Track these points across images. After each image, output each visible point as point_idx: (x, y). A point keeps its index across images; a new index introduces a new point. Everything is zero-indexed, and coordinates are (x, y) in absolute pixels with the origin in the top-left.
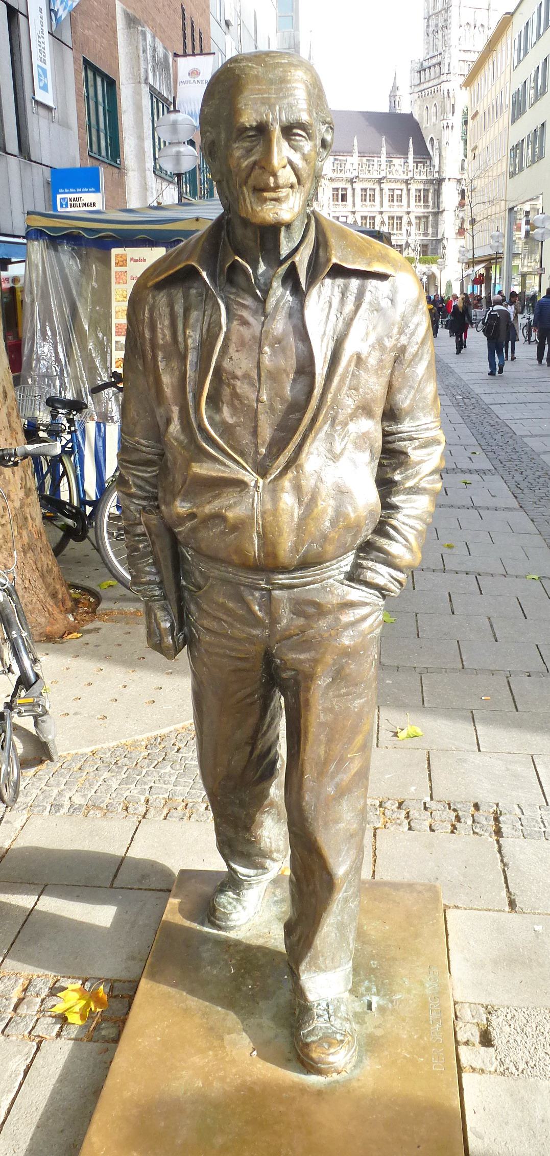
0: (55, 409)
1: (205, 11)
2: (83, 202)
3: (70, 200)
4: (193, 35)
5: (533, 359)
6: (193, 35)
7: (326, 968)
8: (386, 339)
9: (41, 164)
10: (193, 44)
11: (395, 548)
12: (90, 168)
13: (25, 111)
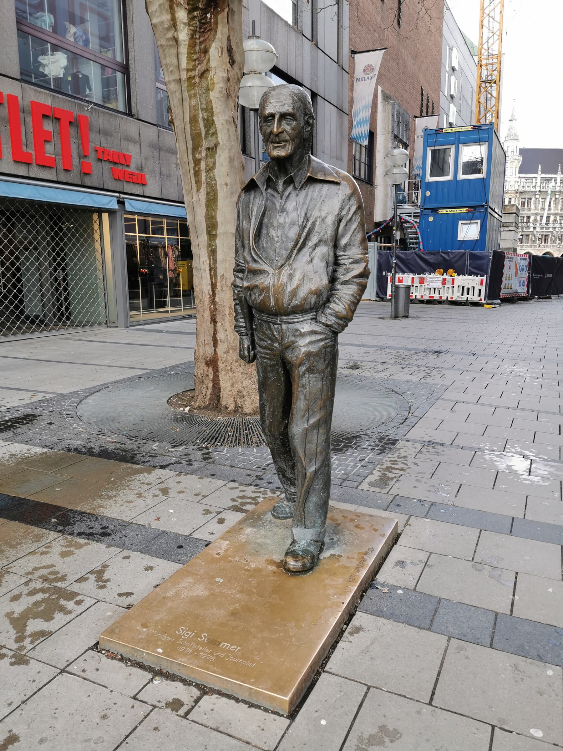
0: (341, 318)
1: (437, 89)
5: (508, 258)
12: (330, 456)
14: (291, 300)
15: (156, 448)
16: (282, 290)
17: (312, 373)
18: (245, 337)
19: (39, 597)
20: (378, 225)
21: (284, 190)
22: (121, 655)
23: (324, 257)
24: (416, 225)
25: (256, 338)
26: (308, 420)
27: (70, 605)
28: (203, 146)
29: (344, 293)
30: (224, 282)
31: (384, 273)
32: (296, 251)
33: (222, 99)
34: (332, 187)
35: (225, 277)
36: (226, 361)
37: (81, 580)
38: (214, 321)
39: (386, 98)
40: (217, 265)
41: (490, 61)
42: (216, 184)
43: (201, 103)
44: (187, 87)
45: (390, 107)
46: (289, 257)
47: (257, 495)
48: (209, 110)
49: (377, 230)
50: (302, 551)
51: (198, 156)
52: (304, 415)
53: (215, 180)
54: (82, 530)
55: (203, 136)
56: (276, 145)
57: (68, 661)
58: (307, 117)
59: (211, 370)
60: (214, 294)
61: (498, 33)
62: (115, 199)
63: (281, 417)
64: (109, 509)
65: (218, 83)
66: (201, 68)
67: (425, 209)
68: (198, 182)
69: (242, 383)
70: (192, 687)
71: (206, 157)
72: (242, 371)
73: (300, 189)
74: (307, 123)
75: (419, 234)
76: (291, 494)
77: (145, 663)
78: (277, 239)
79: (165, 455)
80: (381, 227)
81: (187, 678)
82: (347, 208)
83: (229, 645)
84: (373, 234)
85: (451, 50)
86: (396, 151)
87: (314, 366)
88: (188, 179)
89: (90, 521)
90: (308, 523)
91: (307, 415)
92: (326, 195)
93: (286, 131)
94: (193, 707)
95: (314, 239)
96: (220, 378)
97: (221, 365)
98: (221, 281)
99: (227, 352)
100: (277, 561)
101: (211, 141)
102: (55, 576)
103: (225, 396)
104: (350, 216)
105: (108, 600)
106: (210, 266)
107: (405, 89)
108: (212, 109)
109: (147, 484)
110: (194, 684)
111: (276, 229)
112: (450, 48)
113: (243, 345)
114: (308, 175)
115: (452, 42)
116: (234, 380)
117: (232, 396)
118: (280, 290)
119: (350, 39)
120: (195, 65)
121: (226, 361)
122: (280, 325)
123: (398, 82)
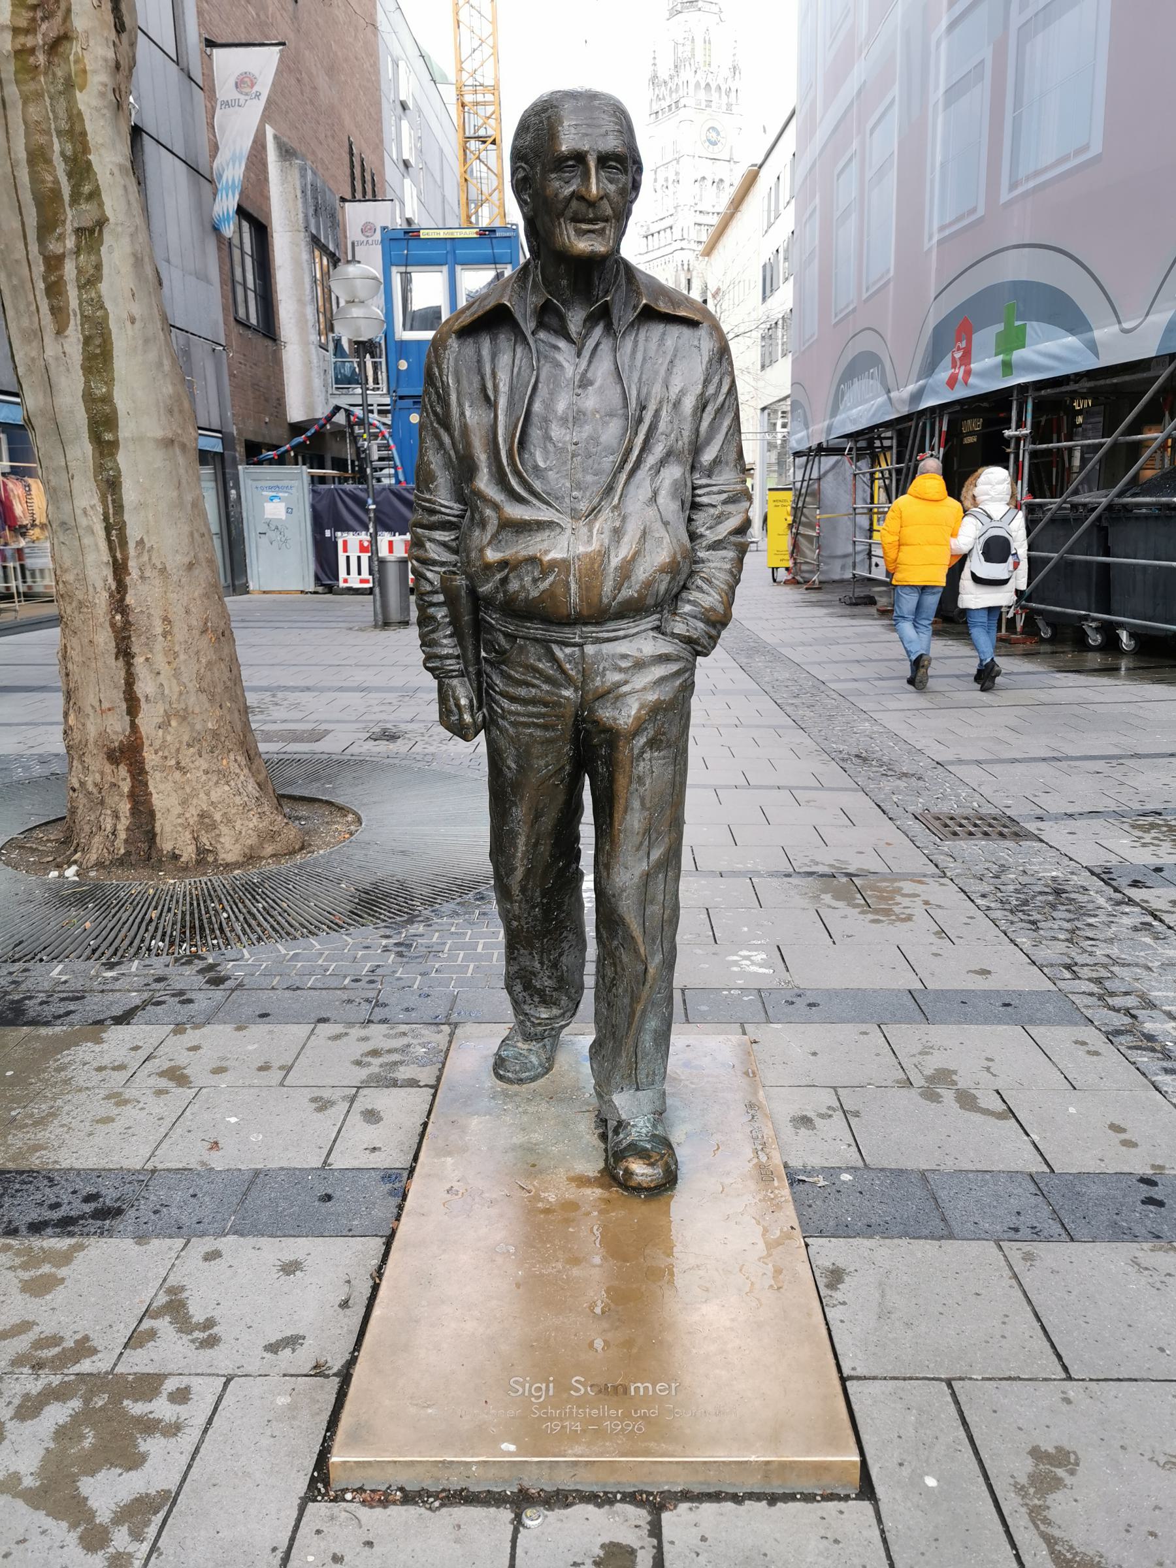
4: (363, 177)
6: (363, 177)
7: (705, 647)
10: (364, 188)
14: (618, 587)
15: (64, 978)
17: (659, 749)
19: (57, 1414)
20: (297, 429)
21: (586, 336)
22: (401, 1489)
23: (676, 486)
24: (386, 432)
26: (649, 854)
27: (161, 1408)
28: (68, 222)
30: (145, 558)
31: (328, 533)
32: (623, 477)
33: (105, 111)
34: (686, 331)
35: (148, 545)
36: (164, 745)
37: (135, 1340)
38: (125, 653)
39: (287, 153)
40: (126, 517)
41: (480, 98)
42: (106, 317)
43: (56, 118)
44: (16, 73)
45: (296, 174)
46: (609, 489)
47: (404, 1041)
48: (76, 134)
49: (301, 438)
50: (649, 1142)
51: (54, 247)
52: (641, 843)
53: (102, 307)
54: (34, 1215)
55: (66, 198)
56: (584, 226)
57: (274, 1549)
59: (123, 771)
60: (122, 587)
61: (490, 41)
63: (551, 856)
64: (64, 1150)
65: (95, 72)
66: (48, 30)
67: (401, 398)
68: (59, 312)
69: (208, 794)
70: (618, 1505)
71: (77, 252)
72: (205, 766)
75: (394, 450)
76: (539, 1024)
77: (475, 1489)
79: (103, 991)
80: (309, 434)
81: (595, 1489)
82: (716, 380)
83: (650, 1386)
84: (293, 448)
85: (396, 64)
87: (664, 734)
88: (29, 304)
89: (38, 1189)
90: (642, 1077)
91: (646, 843)
92: (676, 350)
94: (659, 1548)
95: (658, 450)
96: (151, 789)
97: (150, 757)
98: (139, 556)
99: (164, 725)
100: (591, 1174)
101: (86, 214)
102: (57, 1350)
103: (168, 829)
104: (721, 398)
105: (249, 1369)
106: (106, 518)
108: (84, 134)
109: (114, 1069)
110: (619, 1496)
112: (393, 60)
114: (644, 301)
115: (397, 50)
116: (188, 790)
117: (186, 826)
118: (596, 566)
119: (200, 13)
120: (34, 20)
121: (164, 745)
122: (581, 646)
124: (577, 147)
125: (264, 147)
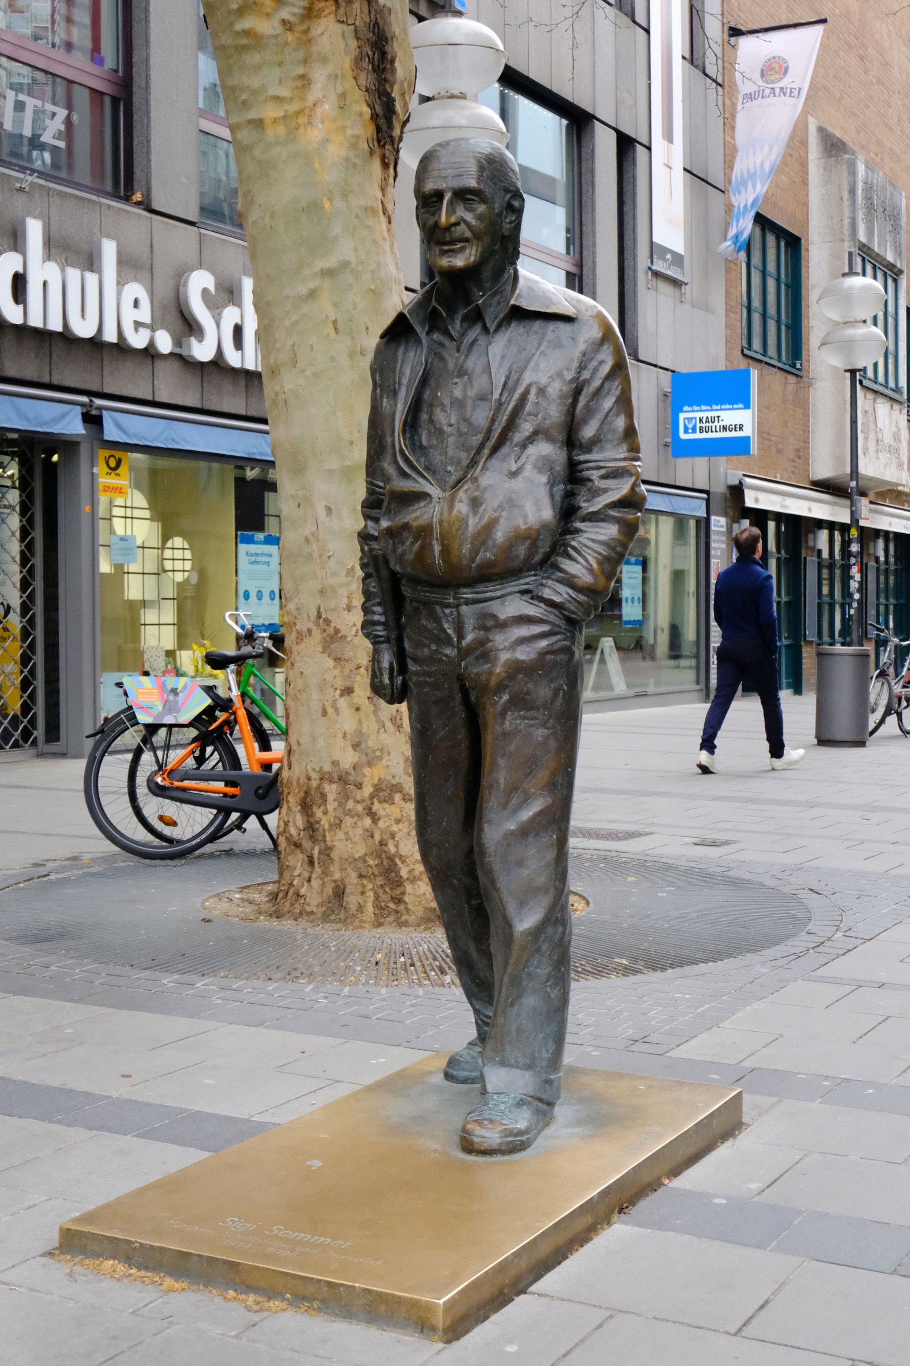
2: (721, 423)
3: (701, 420)
8: (566, 373)
9: (655, 366)
11: (568, 566)
13: (635, 285)
14: (475, 552)
16: (458, 530)
18: (384, 646)
21: (463, 335)
25: (407, 644)
29: (588, 539)
32: (486, 452)
46: (473, 463)
56: (446, 248)
58: (508, 196)
62: (78, 410)
73: (497, 330)
74: (510, 208)
78: (450, 429)
86: (857, 281)
93: (466, 222)
95: (526, 428)
104: (596, 383)
107: (886, 125)
111: (448, 410)
113: (379, 662)
122: (457, 606)
123: (867, 107)
124: (435, 188)
125: (805, 143)
